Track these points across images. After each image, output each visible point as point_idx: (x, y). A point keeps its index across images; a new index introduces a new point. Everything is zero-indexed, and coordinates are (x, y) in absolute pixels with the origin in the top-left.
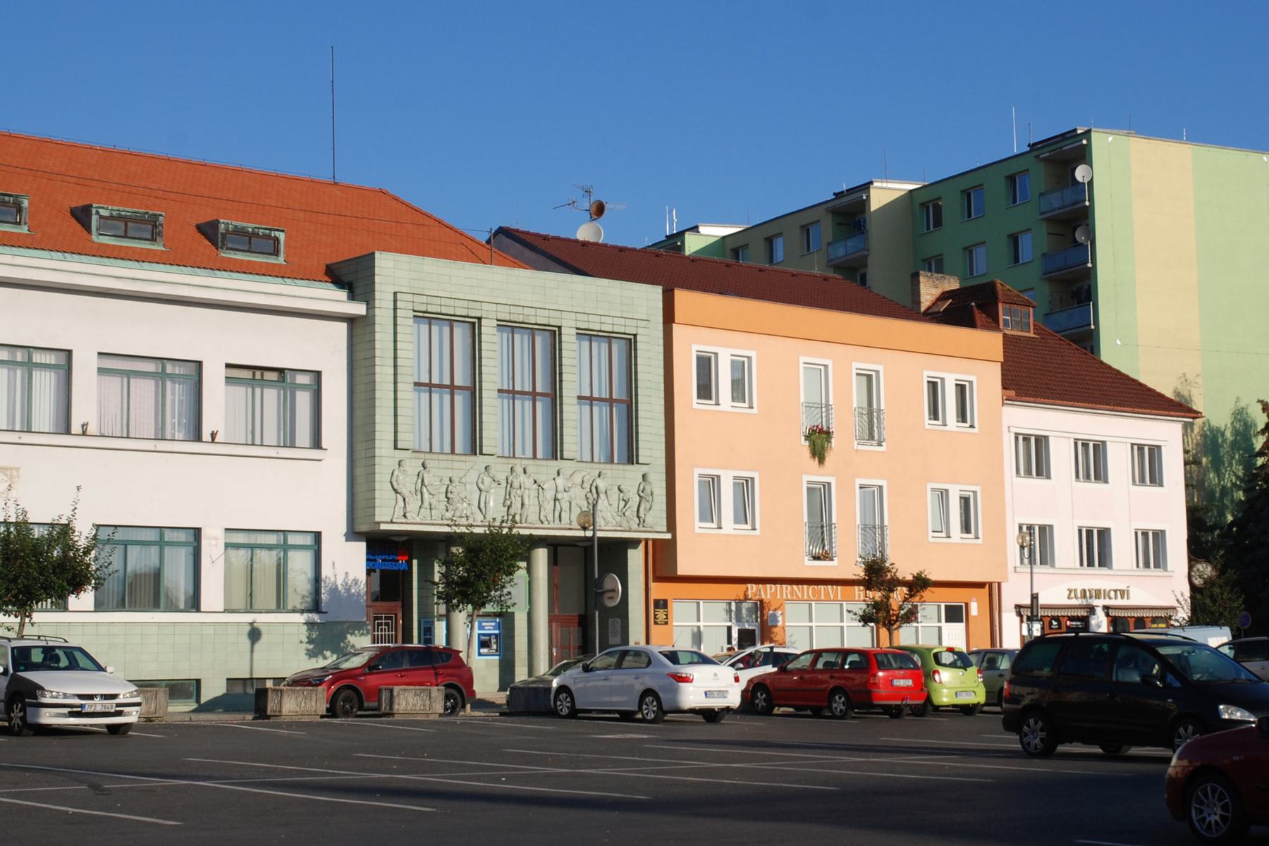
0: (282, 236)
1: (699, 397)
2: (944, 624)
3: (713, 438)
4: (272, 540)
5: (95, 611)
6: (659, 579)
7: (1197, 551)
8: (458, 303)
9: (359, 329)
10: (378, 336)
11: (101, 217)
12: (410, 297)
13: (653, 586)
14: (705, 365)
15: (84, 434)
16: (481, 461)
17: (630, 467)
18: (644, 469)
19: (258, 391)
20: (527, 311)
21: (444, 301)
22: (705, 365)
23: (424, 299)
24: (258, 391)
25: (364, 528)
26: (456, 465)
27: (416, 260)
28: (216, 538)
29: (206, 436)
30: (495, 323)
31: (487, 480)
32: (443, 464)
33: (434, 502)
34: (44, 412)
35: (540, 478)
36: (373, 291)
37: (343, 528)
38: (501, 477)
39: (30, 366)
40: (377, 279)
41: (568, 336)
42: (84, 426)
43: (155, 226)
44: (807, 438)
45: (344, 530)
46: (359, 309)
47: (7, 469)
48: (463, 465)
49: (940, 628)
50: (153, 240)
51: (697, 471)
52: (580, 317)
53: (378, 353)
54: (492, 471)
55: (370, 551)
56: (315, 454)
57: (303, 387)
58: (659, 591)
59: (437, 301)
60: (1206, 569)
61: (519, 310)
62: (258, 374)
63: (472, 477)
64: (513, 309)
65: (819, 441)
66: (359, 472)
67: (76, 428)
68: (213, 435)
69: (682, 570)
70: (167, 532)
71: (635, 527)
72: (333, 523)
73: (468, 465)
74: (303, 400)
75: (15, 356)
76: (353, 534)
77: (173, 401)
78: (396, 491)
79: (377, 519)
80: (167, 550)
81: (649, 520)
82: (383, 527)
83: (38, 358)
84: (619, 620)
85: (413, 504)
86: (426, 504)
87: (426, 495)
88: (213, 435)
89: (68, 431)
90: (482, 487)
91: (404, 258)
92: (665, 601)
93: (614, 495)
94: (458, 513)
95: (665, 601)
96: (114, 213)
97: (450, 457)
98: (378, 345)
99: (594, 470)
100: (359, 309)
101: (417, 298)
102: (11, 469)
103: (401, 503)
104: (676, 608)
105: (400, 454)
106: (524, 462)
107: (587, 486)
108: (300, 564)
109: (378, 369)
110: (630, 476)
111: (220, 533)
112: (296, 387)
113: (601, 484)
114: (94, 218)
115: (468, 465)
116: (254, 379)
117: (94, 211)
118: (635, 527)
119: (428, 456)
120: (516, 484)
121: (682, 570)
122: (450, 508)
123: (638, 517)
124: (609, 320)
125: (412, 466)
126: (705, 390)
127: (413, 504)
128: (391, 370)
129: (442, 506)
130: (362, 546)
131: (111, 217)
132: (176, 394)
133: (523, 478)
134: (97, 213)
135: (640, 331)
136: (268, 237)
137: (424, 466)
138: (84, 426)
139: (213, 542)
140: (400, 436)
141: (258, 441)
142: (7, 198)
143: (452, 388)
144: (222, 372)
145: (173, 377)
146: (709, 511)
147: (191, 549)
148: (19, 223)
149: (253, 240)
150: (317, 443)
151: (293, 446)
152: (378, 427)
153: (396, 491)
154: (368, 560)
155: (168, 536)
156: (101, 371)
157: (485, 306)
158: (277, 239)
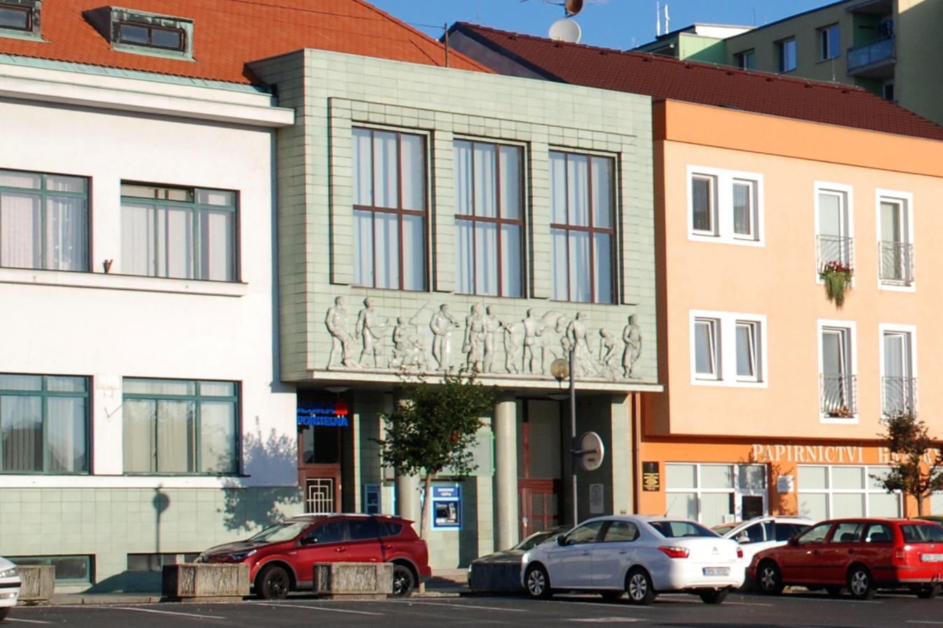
0: (189, 28)
1: (696, 227)
4: (181, 390)
6: (648, 438)
8: (406, 112)
9: (285, 141)
10: (308, 150)
12: (347, 104)
14: (702, 190)
16: (434, 299)
18: (631, 310)
19: (161, 213)
20: (489, 123)
21: (389, 110)
22: (702, 190)
23: (365, 107)
24: (161, 213)
25: (293, 376)
26: (405, 303)
27: (355, 59)
28: (111, 388)
29: (98, 266)
30: (451, 136)
31: (443, 322)
32: (389, 302)
33: (379, 347)
35: (505, 321)
38: (460, 318)
40: (307, 82)
41: (539, 154)
43: (30, 13)
46: (285, 117)
48: (413, 304)
50: (28, 29)
51: (694, 313)
52: (553, 130)
53: (308, 169)
54: (449, 312)
55: (301, 404)
56: (233, 288)
57: (218, 209)
58: (648, 452)
61: (480, 121)
62: (162, 193)
63: (425, 317)
64: (473, 121)
66: (287, 310)
68: (107, 265)
69: (675, 429)
71: (619, 377)
73: (420, 304)
74: (218, 225)
78: (333, 334)
79: (310, 366)
81: (637, 369)
82: (317, 376)
85: (354, 349)
86: (369, 349)
87: (369, 339)
88: (107, 265)
90: (436, 329)
91: (340, 58)
93: (595, 340)
97: (398, 294)
98: (308, 160)
100: (285, 117)
101: (356, 106)
103: (338, 348)
106: (487, 300)
107: (562, 329)
109: (308, 189)
110: (614, 318)
111: (118, 382)
112: (208, 209)
113: (580, 327)
115: (420, 304)
118: (619, 377)
119: (371, 292)
120: (477, 327)
122: (398, 353)
124: (589, 135)
125: (352, 304)
126: (702, 219)
127: (354, 349)
128: (325, 191)
129: (389, 350)
130: (291, 399)
132: (59, 216)
133: (485, 319)
135: (625, 149)
136: (171, 29)
137: (366, 304)
139: (109, 393)
140: (336, 268)
141: (162, 273)
143: (400, 212)
144: (117, 190)
145: (56, 195)
146: (708, 360)
149: (154, 32)
150: (235, 275)
151: (206, 279)
152: (309, 258)
153: (333, 334)
154: (299, 414)
155: (206, 390)
157: (439, 116)
158: (183, 32)
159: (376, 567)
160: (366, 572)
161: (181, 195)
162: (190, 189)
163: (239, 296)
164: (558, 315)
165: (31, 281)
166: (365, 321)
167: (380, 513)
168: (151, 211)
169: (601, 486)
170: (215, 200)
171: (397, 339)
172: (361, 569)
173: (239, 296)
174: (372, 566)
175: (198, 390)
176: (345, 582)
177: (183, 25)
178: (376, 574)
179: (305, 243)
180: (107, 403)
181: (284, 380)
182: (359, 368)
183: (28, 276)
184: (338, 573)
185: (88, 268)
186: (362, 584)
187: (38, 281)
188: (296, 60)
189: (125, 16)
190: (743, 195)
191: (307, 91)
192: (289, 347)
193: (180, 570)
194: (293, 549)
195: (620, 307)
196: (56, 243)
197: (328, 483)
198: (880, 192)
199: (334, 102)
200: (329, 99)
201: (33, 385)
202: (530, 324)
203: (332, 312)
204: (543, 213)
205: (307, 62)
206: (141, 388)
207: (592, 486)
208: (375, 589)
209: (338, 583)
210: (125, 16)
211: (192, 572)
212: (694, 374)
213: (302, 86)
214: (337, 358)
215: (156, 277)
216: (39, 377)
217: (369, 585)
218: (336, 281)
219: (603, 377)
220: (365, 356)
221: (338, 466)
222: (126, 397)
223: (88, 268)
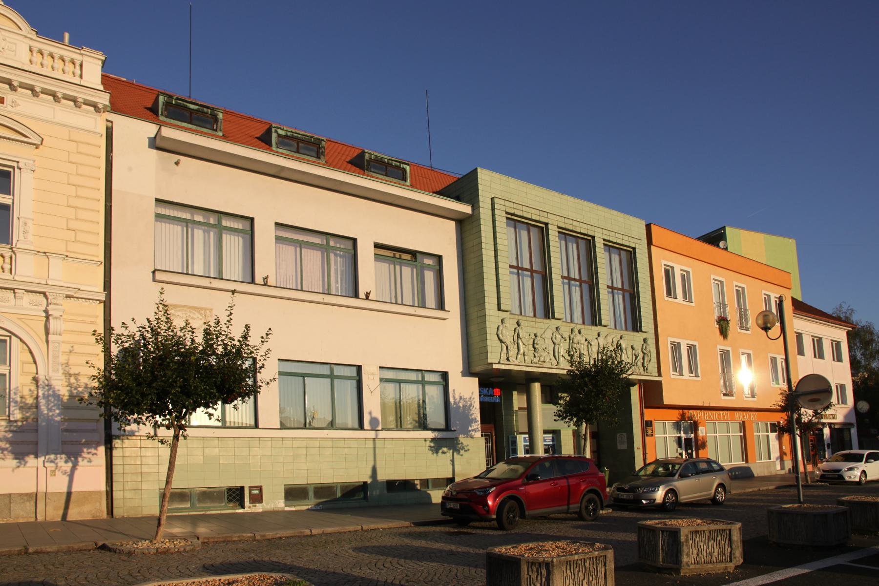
0: (408, 168)
2: (769, 433)
3: (679, 320)
4: (413, 376)
5: (281, 429)
6: (648, 407)
7: (858, 395)
8: (533, 211)
9: (466, 227)
10: (482, 227)
11: (279, 136)
12: (503, 202)
13: (645, 410)
14: (668, 274)
15: (265, 284)
16: (554, 323)
17: (636, 334)
18: (644, 335)
19: (398, 267)
21: (525, 209)
22: (668, 274)
23: (512, 205)
24: (398, 267)
25: (478, 369)
26: (538, 325)
27: (504, 178)
28: (373, 374)
29: (362, 295)
31: (558, 336)
34: (234, 266)
35: (589, 338)
36: (478, 195)
37: (460, 368)
38: (566, 335)
39: (220, 229)
40: (480, 187)
41: (599, 244)
42: (266, 279)
43: (319, 148)
44: (718, 323)
45: (461, 369)
46: (467, 209)
47: (202, 309)
48: (542, 326)
49: (768, 436)
51: (670, 339)
53: (483, 240)
54: (560, 331)
55: (481, 385)
56: (440, 314)
57: (429, 267)
58: (649, 414)
59: (520, 207)
60: (864, 406)
62: (397, 255)
63: (548, 335)
65: (723, 324)
66: (473, 328)
67: (259, 279)
68: (367, 295)
69: (666, 401)
70: (335, 367)
71: (642, 372)
72: (454, 364)
74: (430, 277)
75: (209, 219)
76: (468, 371)
77: (336, 270)
78: (501, 341)
79: (490, 361)
80: (329, 380)
82: (495, 366)
83: (226, 223)
84: (625, 434)
85: (513, 352)
86: (522, 351)
87: (521, 344)
88: (367, 295)
89: (253, 281)
91: (497, 175)
92: (651, 422)
94: (542, 359)
95: (651, 422)
96: (289, 134)
98: (483, 234)
99: (618, 333)
100: (467, 209)
101: (507, 204)
102: (205, 309)
103: (505, 348)
104: (657, 426)
105: (502, 315)
107: (615, 344)
108: (434, 393)
109: (484, 251)
110: (636, 339)
111: (376, 370)
112: (424, 267)
114: (274, 135)
116: (394, 257)
117: (273, 130)
119: (520, 317)
120: (575, 341)
121: (666, 401)
122: (537, 355)
123: (643, 366)
125: (511, 324)
126: (670, 291)
127: (513, 352)
128: (493, 253)
130: (476, 380)
131: (286, 137)
132: (337, 265)
134: (276, 132)
136: (398, 167)
137: (518, 324)
138: (266, 279)
139: (371, 377)
140: (502, 301)
142: (205, 110)
143: (531, 270)
144: (272, 231)
145: (335, 248)
146: (677, 366)
147: (354, 383)
148: (216, 130)
149: (389, 168)
150: (441, 306)
152: (486, 294)
153: (501, 341)
155: (338, 371)
156: (278, 239)
158: (404, 170)
159: (730, 530)
160: (719, 538)
161: (407, 257)
162: (414, 254)
163: (444, 319)
165: (321, 301)
166: (518, 335)
167: (560, 452)
168: (392, 266)
169: (625, 434)
170: (428, 261)
171: (536, 346)
172: (714, 535)
173: (444, 319)
174: (723, 531)
175: (423, 377)
176: (695, 552)
177: (405, 166)
178: (730, 540)
179: (483, 285)
180: (370, 382)
181: (473, 371)
182: (516, 362)
183: (319, 298)
184: (687, 541)
185: (356, 295)
186: (716, 554)
187: (326, 301)
188: (472, 177)
189: (373, 157)
190: (685, 279)
191: (480, 193)
192: (475, 350)
193: (524, 567)
194: (521, 485)
195: (640, 333)
196: (337, 282)
197: (488, 435)
198: (735, 283)
199: (496, 200)
200: (492, 199)
201: (326, 370)
202: (601, 340)
203: (501, 328)
204: (604, 280)
205: (479, 175)
206: (390, 375)
207: (618, 435)
208: (731, 561)
209: (688, 555)
210: (373, 157)
211: (544, 572)
212: (672, 373)
213: (477, 190)
214: (504, 356)
215: (396, 303)
216: (328, 366)
217: (723, 554)
218: (502, 308)
220: (519, 356)
221: (492, 425)
222: (381, 380)
223: (356, 295)
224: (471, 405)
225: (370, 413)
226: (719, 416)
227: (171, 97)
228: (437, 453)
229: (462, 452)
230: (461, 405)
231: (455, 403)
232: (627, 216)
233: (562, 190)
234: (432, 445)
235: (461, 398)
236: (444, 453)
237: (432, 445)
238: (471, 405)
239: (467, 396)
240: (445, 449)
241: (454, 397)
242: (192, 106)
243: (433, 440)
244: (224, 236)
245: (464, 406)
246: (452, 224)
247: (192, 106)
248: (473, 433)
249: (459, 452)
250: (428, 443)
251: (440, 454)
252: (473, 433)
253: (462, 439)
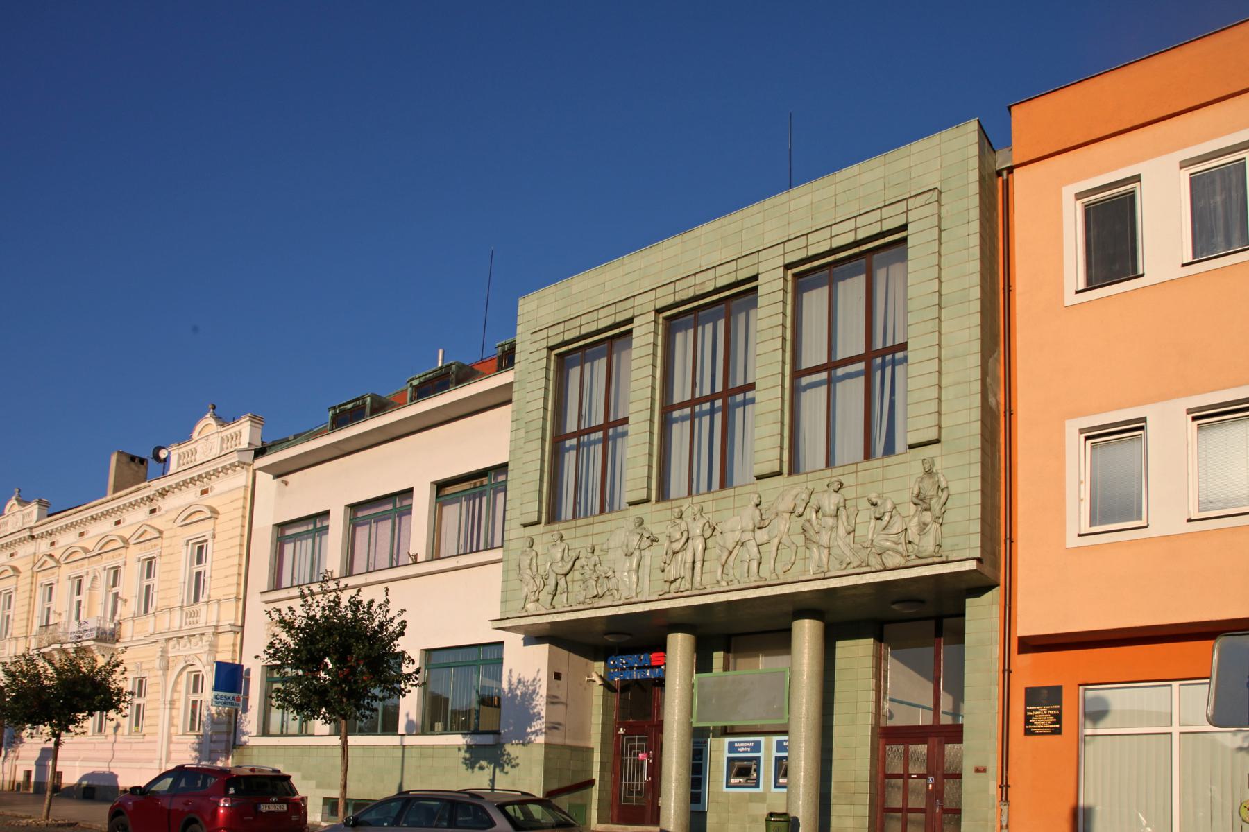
157: (638, 300)
164: (794, 492)
219: (868, 566)
224: (534, 691)
225: (407, 715)
226: (514, 784)
227: (334, 408)
228: (473, 768)
229: (507, 768)
230: (519, 692)
231: (510, 690)
232: (892, 155)
233: (792, 177)
234: (468, 756)
235: (519, 681)
236: (482, 768)
237: (468, 756)
238: (534, 691)
239: (528, 677)
240: (484, 763)
241: (510, 681)
242: (349, 406)
243: (469, 747)
244: (803, 367)
245: (524, 694)
246: (805, 295)
247: (349, 406)
248: (533, 737)
249: (502, 770)
250: (462, 754)
251: (476, 769)
252: (533, 737)
253: (512, 749)
